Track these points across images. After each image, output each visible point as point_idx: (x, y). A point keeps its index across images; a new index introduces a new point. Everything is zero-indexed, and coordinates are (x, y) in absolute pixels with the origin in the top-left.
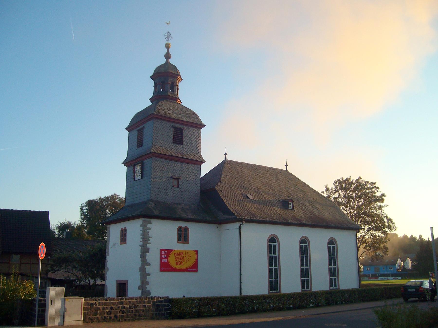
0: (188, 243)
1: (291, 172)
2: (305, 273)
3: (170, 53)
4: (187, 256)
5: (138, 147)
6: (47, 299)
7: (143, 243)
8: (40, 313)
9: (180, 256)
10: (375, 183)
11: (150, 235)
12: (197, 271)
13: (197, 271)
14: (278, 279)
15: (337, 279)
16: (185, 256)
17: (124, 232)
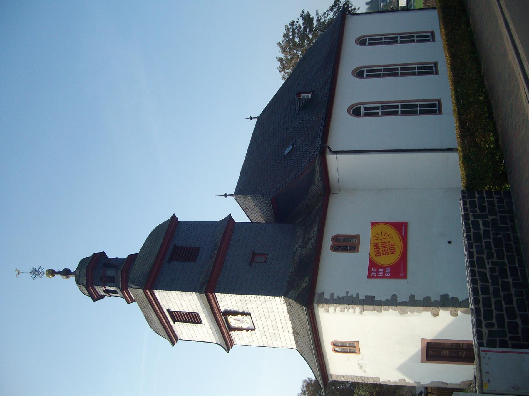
1: (261, 112)
3: (61, 270)
4: (381, 237)
5: (201, 323)
9: (380, 247)
11: (344, 295)
12: (406, 224)
13: (406, 224)
14: (418, 103)
16: (380, 241)
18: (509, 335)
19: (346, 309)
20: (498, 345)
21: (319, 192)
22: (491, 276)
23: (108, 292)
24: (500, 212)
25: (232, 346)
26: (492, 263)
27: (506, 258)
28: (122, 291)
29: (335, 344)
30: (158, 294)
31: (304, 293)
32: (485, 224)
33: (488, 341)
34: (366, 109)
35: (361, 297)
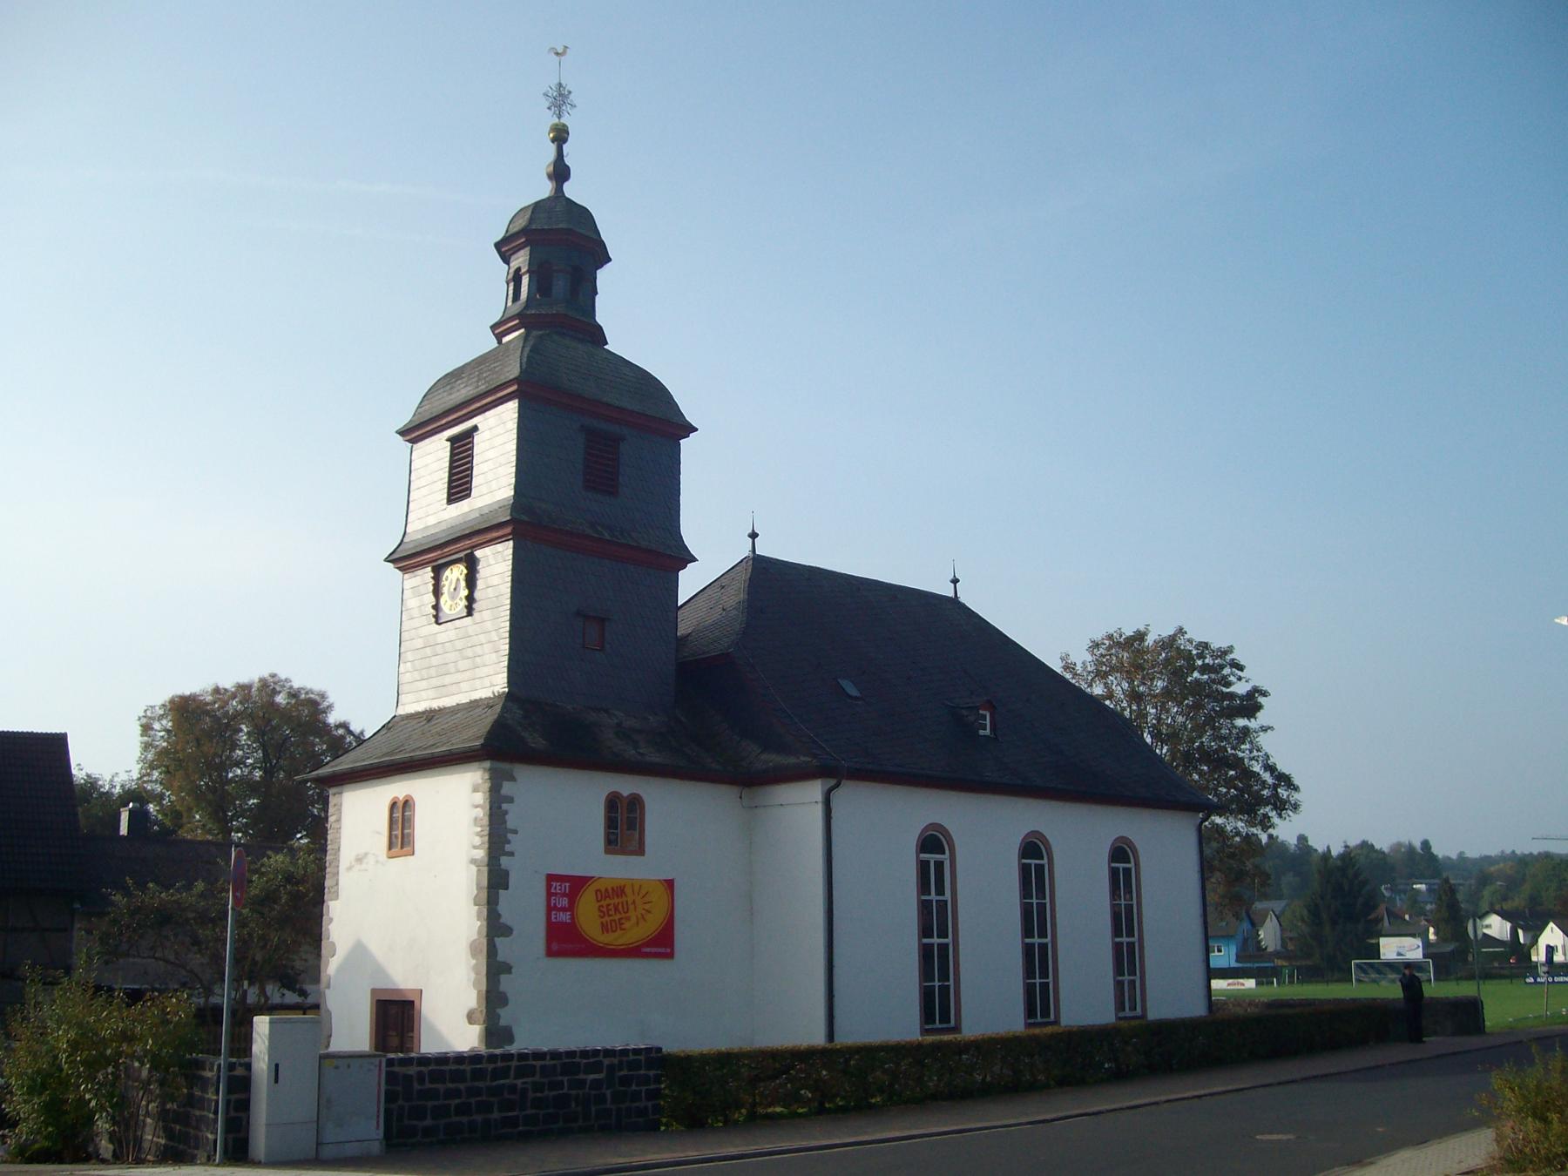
2: (1038, 961)
5: (450, 501)
8: (232, 1114)
9: (616, 901)
10: (1230, 649)
11: (510, 825)
12: (670, 955)
13: (670, 955)
23: (516, 278)
25: (403, 569)
26: (524, 1091)
28: (518, 316)
29: (407, 804)
30: (512, 407)
31: (518, 738)
32: (597, 1084)
35: (504, 861)
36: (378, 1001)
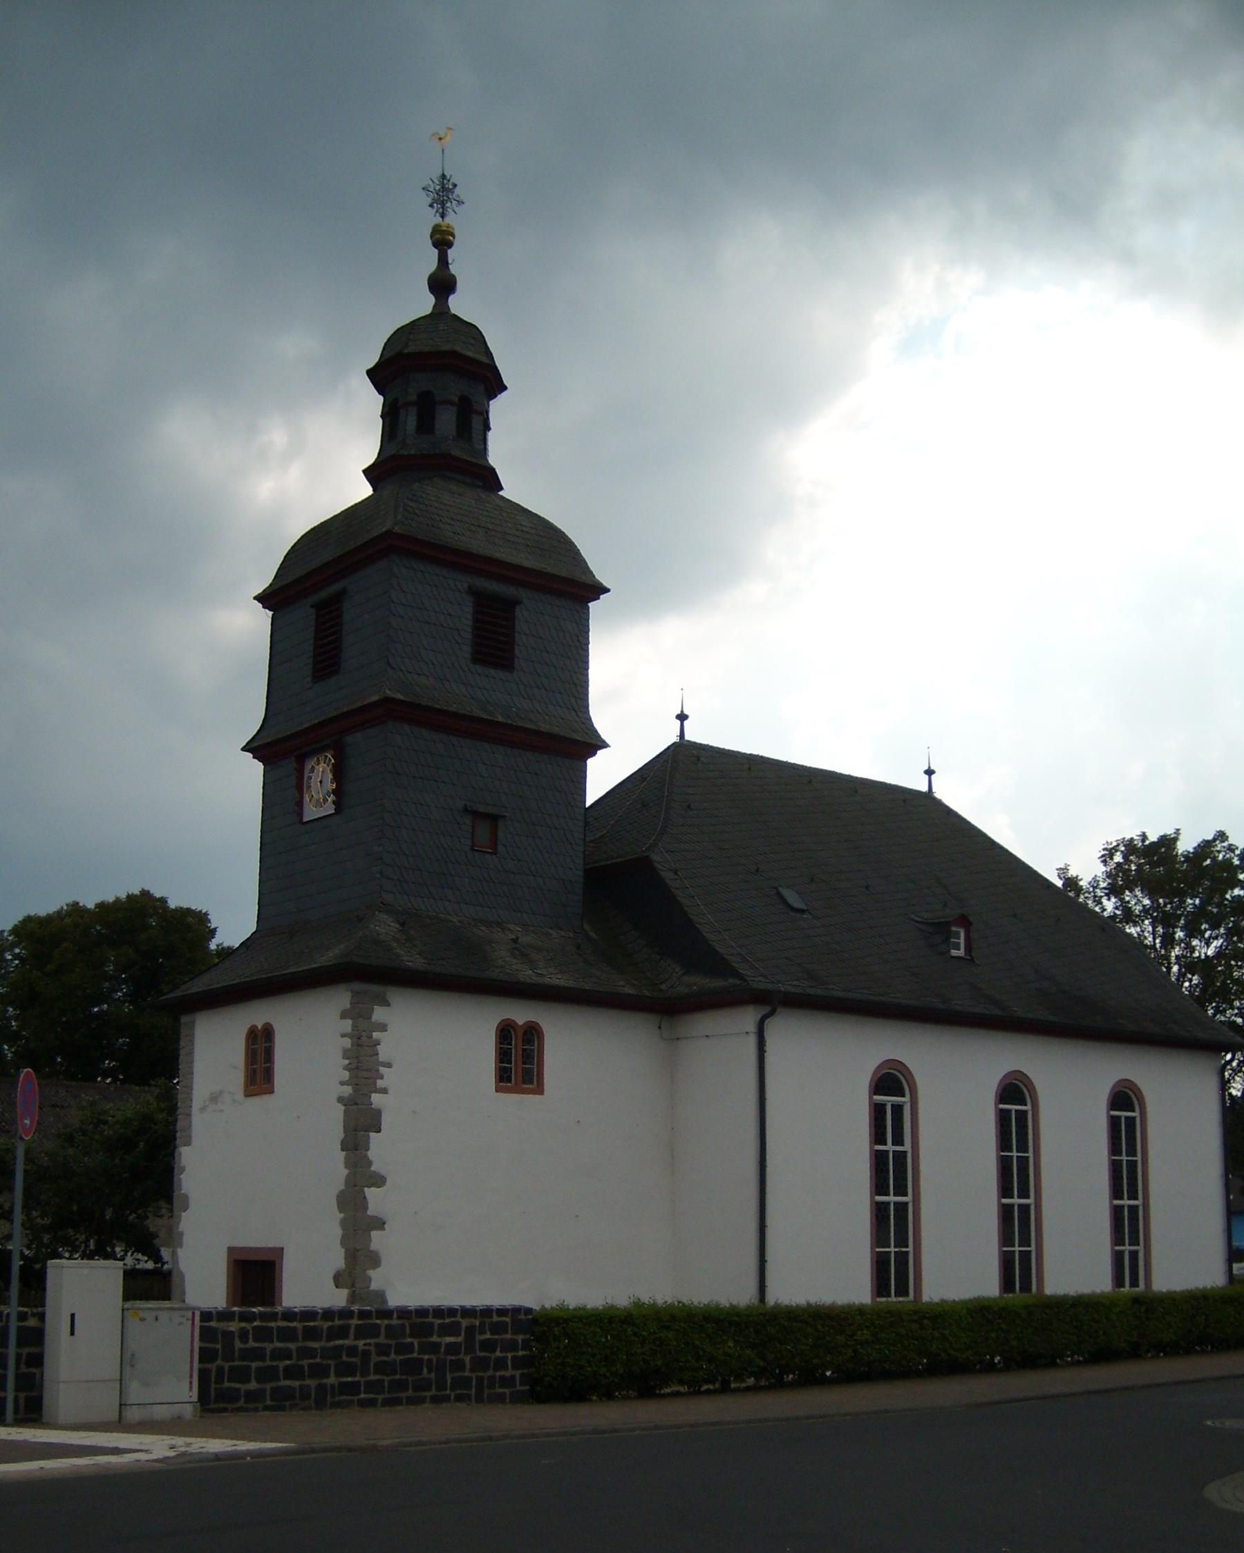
0: (540, 1090)
2: (1018, 1225)
3: (453, 269)
6: (49, 1310)
7: (355, 1090)
8: (23, 1369)
15: (1141, 1255)
17: (260, 1048)
18: (227, 1366)
19: (347, 1062)
20: (204, 1345)
21: (664, 987)
22: (341, 1347)
24: (480, 1380)
26: (366, 1354)
27: (378, 1377)
33: (214, 1330)
34: (898, 1109)
36: (236, 1261)
